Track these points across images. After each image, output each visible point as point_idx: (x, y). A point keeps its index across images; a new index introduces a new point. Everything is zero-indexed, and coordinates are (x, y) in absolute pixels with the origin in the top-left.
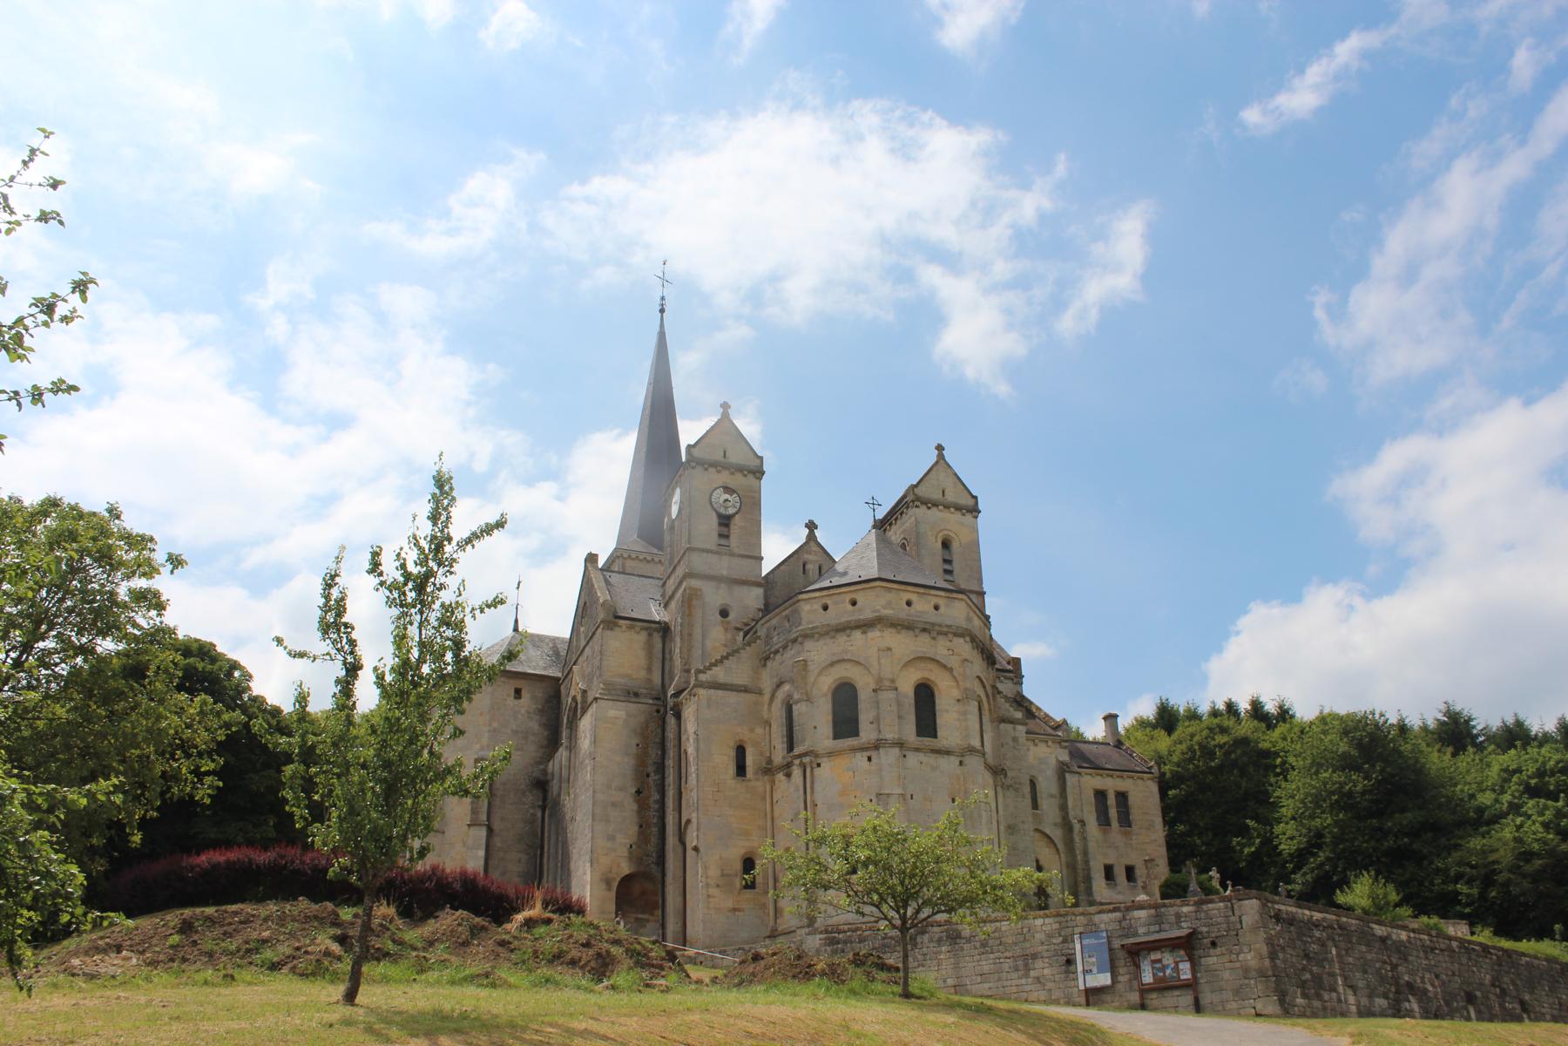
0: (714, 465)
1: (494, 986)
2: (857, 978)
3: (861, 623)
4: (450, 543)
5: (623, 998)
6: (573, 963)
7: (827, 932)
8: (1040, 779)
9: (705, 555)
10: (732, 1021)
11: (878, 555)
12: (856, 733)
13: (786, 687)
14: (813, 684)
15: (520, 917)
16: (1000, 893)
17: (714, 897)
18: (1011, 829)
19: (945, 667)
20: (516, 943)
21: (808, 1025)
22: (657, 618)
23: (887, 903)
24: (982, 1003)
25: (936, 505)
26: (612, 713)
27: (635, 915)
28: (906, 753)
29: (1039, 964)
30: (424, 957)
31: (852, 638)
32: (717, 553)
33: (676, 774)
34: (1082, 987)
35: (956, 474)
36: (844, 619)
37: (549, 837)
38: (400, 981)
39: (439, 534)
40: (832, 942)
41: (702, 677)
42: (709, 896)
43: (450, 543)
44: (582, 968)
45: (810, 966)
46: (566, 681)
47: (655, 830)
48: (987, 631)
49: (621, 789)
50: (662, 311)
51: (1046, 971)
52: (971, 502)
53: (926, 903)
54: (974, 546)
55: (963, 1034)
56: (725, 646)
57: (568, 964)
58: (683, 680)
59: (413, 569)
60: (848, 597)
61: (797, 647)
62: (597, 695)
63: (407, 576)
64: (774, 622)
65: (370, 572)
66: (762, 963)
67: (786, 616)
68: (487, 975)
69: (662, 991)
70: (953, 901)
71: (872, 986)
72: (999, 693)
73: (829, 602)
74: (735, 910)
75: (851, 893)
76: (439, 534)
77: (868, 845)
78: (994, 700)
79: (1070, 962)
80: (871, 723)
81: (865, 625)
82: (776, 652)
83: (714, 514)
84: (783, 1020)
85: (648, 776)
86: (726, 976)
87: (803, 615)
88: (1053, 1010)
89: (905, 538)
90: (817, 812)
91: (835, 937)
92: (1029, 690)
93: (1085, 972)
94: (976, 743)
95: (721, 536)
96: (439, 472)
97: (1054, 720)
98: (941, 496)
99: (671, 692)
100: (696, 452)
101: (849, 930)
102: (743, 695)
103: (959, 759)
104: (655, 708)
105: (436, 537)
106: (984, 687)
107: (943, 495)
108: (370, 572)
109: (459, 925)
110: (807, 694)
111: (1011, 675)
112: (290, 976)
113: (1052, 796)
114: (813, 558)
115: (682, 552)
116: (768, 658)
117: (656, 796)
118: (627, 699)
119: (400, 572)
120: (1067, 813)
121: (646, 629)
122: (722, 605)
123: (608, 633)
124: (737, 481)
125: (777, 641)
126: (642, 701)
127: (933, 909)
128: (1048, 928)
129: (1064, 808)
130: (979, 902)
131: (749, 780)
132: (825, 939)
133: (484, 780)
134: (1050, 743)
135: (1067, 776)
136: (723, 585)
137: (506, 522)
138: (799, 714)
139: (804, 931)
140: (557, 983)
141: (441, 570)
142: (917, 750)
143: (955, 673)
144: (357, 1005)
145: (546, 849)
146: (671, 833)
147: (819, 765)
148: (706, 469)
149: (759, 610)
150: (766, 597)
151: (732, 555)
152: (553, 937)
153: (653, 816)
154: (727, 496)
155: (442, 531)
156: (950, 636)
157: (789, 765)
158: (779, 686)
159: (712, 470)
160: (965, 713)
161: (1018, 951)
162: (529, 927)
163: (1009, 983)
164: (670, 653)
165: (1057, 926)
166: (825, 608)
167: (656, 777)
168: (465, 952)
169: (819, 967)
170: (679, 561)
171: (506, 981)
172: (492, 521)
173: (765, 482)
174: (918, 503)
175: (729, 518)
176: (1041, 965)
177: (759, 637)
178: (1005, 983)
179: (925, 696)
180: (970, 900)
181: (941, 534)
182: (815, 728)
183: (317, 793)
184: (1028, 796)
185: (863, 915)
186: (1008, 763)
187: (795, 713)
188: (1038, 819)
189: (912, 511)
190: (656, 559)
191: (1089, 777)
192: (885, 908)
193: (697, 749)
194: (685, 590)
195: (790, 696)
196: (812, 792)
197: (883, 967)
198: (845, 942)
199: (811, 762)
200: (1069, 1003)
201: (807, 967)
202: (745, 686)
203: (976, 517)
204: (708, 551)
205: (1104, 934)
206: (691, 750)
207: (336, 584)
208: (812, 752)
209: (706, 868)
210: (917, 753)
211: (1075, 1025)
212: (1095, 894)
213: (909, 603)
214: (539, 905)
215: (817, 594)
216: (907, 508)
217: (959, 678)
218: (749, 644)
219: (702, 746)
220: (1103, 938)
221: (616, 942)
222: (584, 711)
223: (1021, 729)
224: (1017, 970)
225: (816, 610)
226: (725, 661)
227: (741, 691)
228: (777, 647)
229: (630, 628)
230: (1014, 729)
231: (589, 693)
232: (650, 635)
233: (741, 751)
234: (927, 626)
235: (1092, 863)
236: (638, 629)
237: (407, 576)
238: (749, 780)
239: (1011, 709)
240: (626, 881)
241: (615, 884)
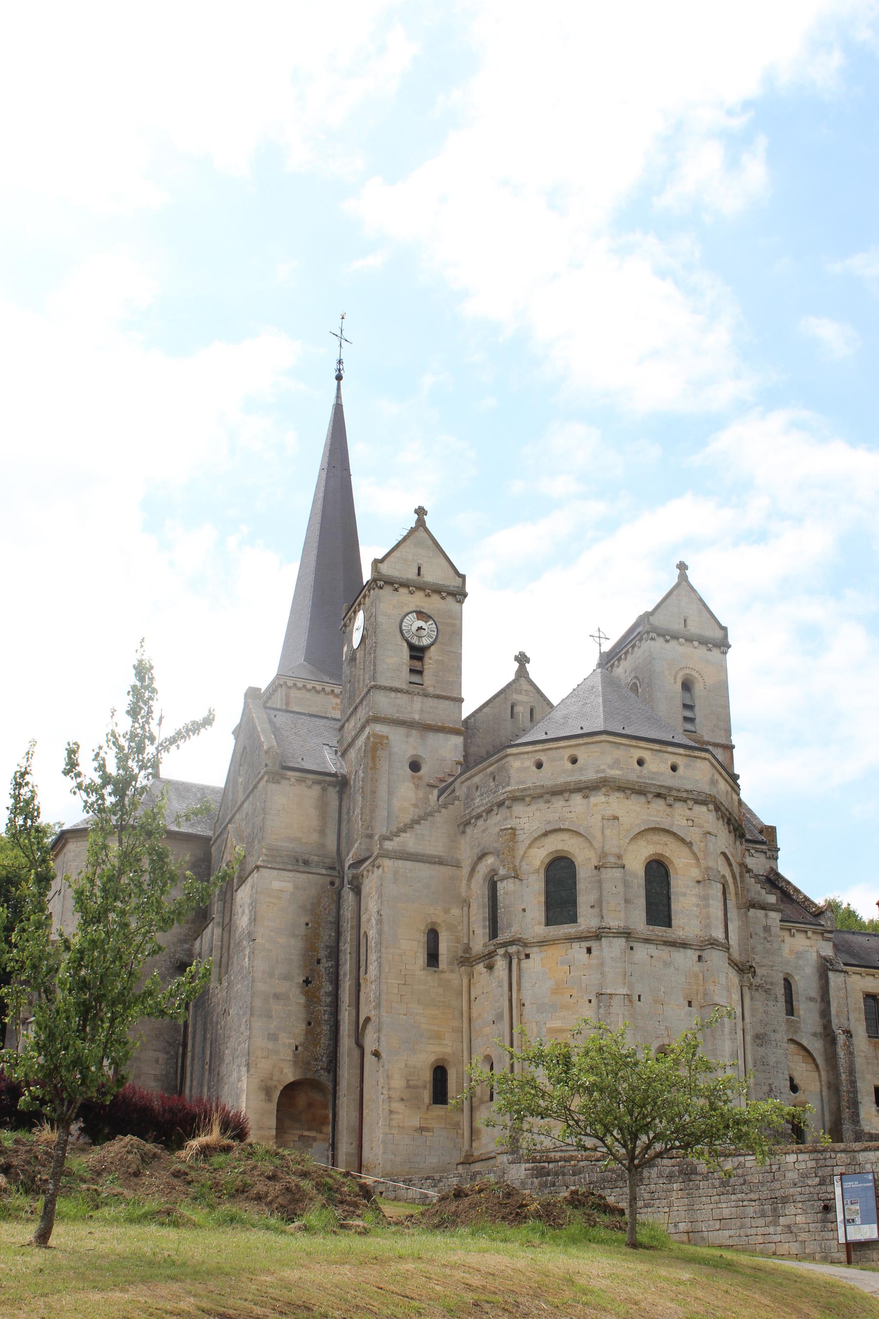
0: (405, 584)
1: (176, 1224)
2: (577, 1220)
3: (582, 785)
4: (152, 743)
5: (318, 1240)
6: (259, 1198)
7: (534, 1160)
8: (797, 978)
9: (393, 695)
10: (448, 1271)
11: (604, 701)
12: (573, 919)
13: (490, 860)
14: (523, 857)
15: (195, 1143)
16: (744, 1129)
17: (398, 1113)
18: (760, 1039)
19: (683, 840)
20: (193, 1173)
21: (530, 1279)
22: (333, 770)
23: (612, 1135)
24: (721, 1256)
25: (675, 637)
26: (276, 885)
27: (300, 1132)
28: (632, 944)
29: (790, 1209)
30: (96, 1190)
31: (571, 802)
33: (354, 961)
34: (842, 1240)
35: (701, 600)
36: (561, 780)
37: (194, 1033)
38: (75, 1219)
39: (139, 731)
40: (540, 1173)
41: (388, 845)
42: (391, 1112)
43: (152, 743)
44: (269, 1204)
45: (522, 1206)
46: (219, 841)
47: (325, 1028)
48: (735, 797)
49: (286, 977)
50: (339, 378)
51: (799, 1219)
52: (719, 634)
53: (657, 1137)
54: (721, 689)
55: (699, 1294)
56: (416, 806)
57: (255, 1199)
58: (363, 847)
59: (112, 769)
60: (567, 753)
61: (503, 811)
62: (259, 863)
63: (107, 779)
64: (476, 779)
65: (66, 773)
66: (466, 1201)
67: (492, 773)
68: (168, 1213)
69: (360, 1233)
70: (689, 1135)
71: (593, 1232)
72: (749, 871)
73: (543, 758)
74: (422, 1129)
75: (571, 1123)
76: (139, 731)
77: (592, 1069)
78: (742, 882)
79: (828, 1208)
80: (592, 907)
81: (586, 788)
82: (479, 817)
83: (405, 644)
84: (502, 1271)
85: (319, 962)
86: (422, 1214)
87: (512, 772)
88: (805, 1268)
89: (636, 677)
90: (524, 1013)
91: (544, 1167)
92: (786, 868)
93: (846, 1222)
94: (719, 935)
95: (412, 671)
96: (140, 662)
97: (816, 905)
98: (682, 625)
99: (349, 861)
100: (384, 568)
101: (562, 1159)
102: (437, 867)
103: (698, 953)
104: (329, 879)
105: (137, 735)
106: (730, 865)
107: (685, 626)
108: (66, 773)
109: (128, 1152)
110: (515, 871)
111: (764, 847)
113: (811, 999)
114: (523, 700)
115: (365, 690)
116: (467, 824)
117: (328, 988)
118: (295, 867)
119: (98, 774)
120: (830, 1021)
121: (319, 782)
123: (273, 786)
124: (433, 604)
125: (480, 802)
126: (314, 870)
127: (666, 1144)
129: (825, 1013)
130: (719, 1138)
131: (443, 972)
132: (533, 1169)
133: (181, 999)
134: (810, 934)
135: (831, 974)
136: (414, 732)
137: (213, 719)
138: (506, 894)
139: (505, 1158)
140: (242, 1221)
141: (143, 773)
142: (647, 941)
143: (695, 848)
144: (49, 1247)
145: (189, 1048)
146: (346, 1033)
147: (527, 956)
148: (396, 590)
149: (458, 763)
150: (466, 746)
151: (426, 695)
152: (235, 1168)
153: (323, 1011)
154: (421, 623)
155: (143, 728)
156: (690, 803)
157: (491, 955)
158: (482, 857)
159: (403, 591)
160: (705, 898)
161: (766, 1194)
162: (205, 1156)
163: (753, 1231)
164: (348, 812)
165: (812, 1164)
166: (539, 765)
167: (330, 964)
168: (136, 1184)
169: (532, 1208)
170: (361, 701)
171: (189, 1220)
172: (199, 718)
173: (468, 608)
174: (654, 635)
176: (793, 1211)
177: (457, 798)
178: (749, 1232)
180: (710, 1135)
181: (681, 674)
182: (524, 910)
183: (7, 1016)
184: (782, 999)
185: (586, 1149)
186: (757, 958)
187: (500, 892)
188: (793, 1027)
189: (646, 645)
190: (328, 689)
191: (858, 977)
192: (609, 1140)
193: (380, 933)
194: (368, 738)
195: (493, 872)
196: (519, 990)
197: (606, 1209)
198: (556, 1174)
200: (827, 1259)
201: (519, 1207)
202: (439, 857)
203: (725, 653)
205: (870, 1177)
206: (372, 933)
207: (27, 784)
208: (519, 940)
210: (647, 946)
211: (831, 1288)
212: (862, 1122)
213: (640, 762)
214: (216, 1130)
215: (529, 748)
216: (641, 640)
217: (700, 855)
218: (445, 806)
219: (386, 928)
220: (868, 1181)
221: (304, 1175)
222: (242, 881)
223: (775, 916)
224: (763, 1216)
225: (528, 768)
226: (416, 826)
227: (434, 863)
228: (479, 811)
229: (300, 781)
230: (766, 916)
231: (249, 859)
232: (324, 790)
233: (433, 936)
234: (662, 791)
235: (859, 1084)
236: (309, 783)
237: (107, 779)
238: (443, 972)
239: (763, 891)
240: (290, 1090)
241: (277, 1094)
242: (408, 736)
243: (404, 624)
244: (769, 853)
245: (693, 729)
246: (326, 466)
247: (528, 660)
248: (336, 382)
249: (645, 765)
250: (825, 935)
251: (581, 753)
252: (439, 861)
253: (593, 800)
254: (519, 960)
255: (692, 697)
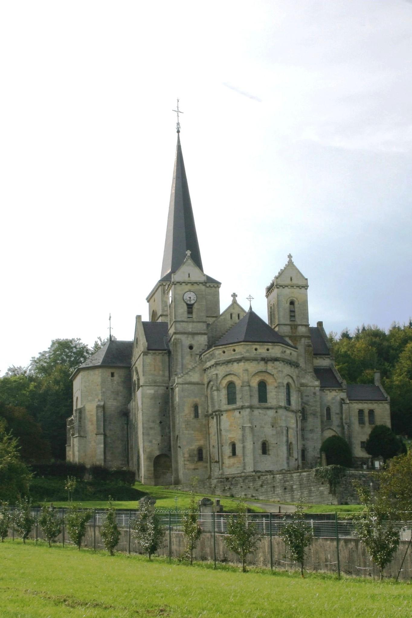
9: (182, 323)
17: (187, 465)
19: (270, 374)
28: (253, 410)
32: (187, 322)
49: (153, 422)
50: (178, 132)
54: (305, 304)
73: (225, 350)
74: (194, 469)
83: (185, 304)
103: (276, 410)
112: (242, 573)
122: (190, 344)
123: (145, 357)
128: (280, 478)
134: (337, 391)
135: (343, 405)
136: (190, 336)
142: (258, 408)
143: (275, 376)
151: (193, 322)
163: (269, 495)
166: (224, 352)
175: (192, 305)
179: (262, 386)
181: (289, 300)
182: (221, 400)
199: (219, 414)
203: (307, 289)
204: (183, 321)
209: (184, 454)
210: (258, 410)
222: (138, 389)
233: (196, 407)
236: (157, 354)
240: (158, 457)
242: (187, 337)
243: (184, 297)
244: (331, 358)
245: (294, 320)
246: (175, 177)
247: (236, 296)
248: (177, 134)
249: (258, 350)
250: (343, 390)
251: (237, 349)
252: (198, 384)
253: (240, 364)
254: (220, 416)
255: (294, 307)
